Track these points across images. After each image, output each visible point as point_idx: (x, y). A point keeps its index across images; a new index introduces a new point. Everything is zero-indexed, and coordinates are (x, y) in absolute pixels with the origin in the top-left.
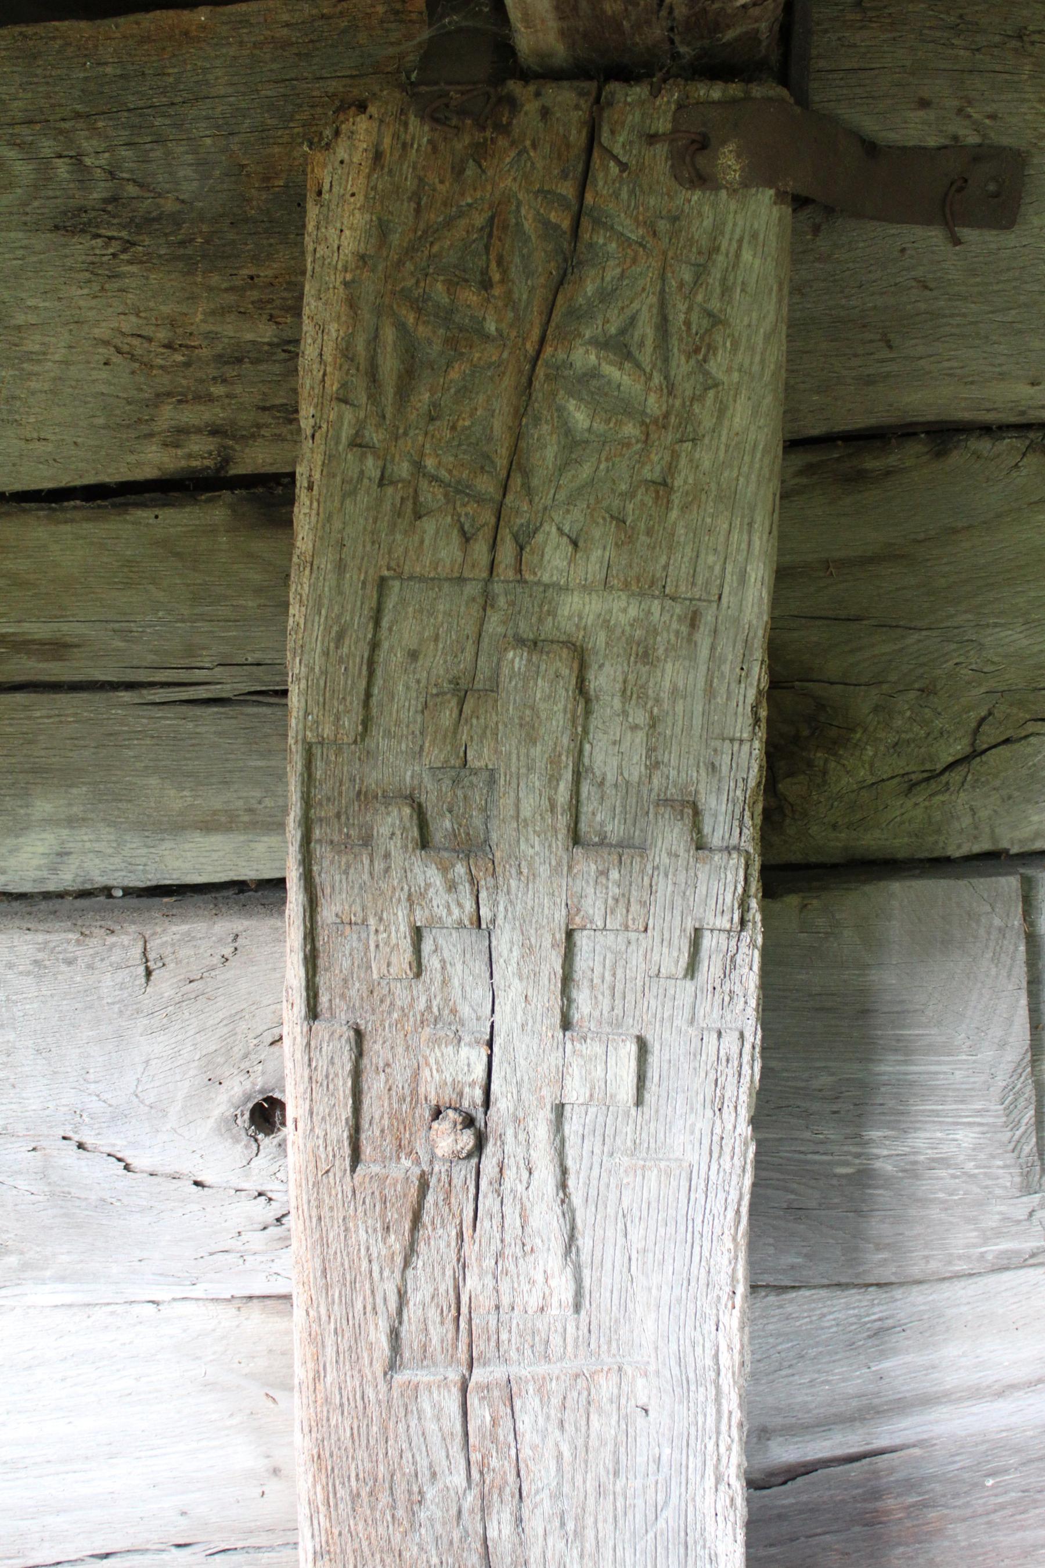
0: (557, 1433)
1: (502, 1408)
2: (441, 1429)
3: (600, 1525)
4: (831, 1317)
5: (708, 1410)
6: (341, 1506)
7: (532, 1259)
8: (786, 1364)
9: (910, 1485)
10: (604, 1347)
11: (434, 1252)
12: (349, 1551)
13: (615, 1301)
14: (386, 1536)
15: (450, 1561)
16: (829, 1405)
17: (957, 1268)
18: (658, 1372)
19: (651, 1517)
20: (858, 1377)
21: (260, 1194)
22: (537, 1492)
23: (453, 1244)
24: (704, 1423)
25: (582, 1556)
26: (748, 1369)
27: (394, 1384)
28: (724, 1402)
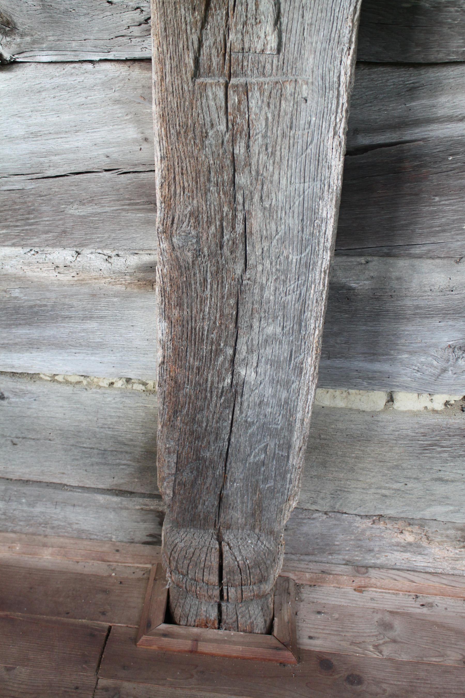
0: (267, 108)
1: (243, 96)
2: (216, 104)
3: (283, 150)
4: (391, 81)
5: (333, 102)
6: (172, 137)
7: (259, 26)
8: (369, 101)
9: (416, 157)
10: (290, 71)
11: (215, 21)
12: (176, 156)
13: (296, 49)
14: (191, 151)
15: (218, 162)
16: (386, 120)
17: (451, 58)
18: (312, 83)
19: (305, 148)
20: (400, 109)
21: (138, 8)
22: (256, 135)
23: (224, 18)
24: (331, 107)
25: (274, 163)
26: (353, 86)
27: (196, 84)
28: (341, 99)
